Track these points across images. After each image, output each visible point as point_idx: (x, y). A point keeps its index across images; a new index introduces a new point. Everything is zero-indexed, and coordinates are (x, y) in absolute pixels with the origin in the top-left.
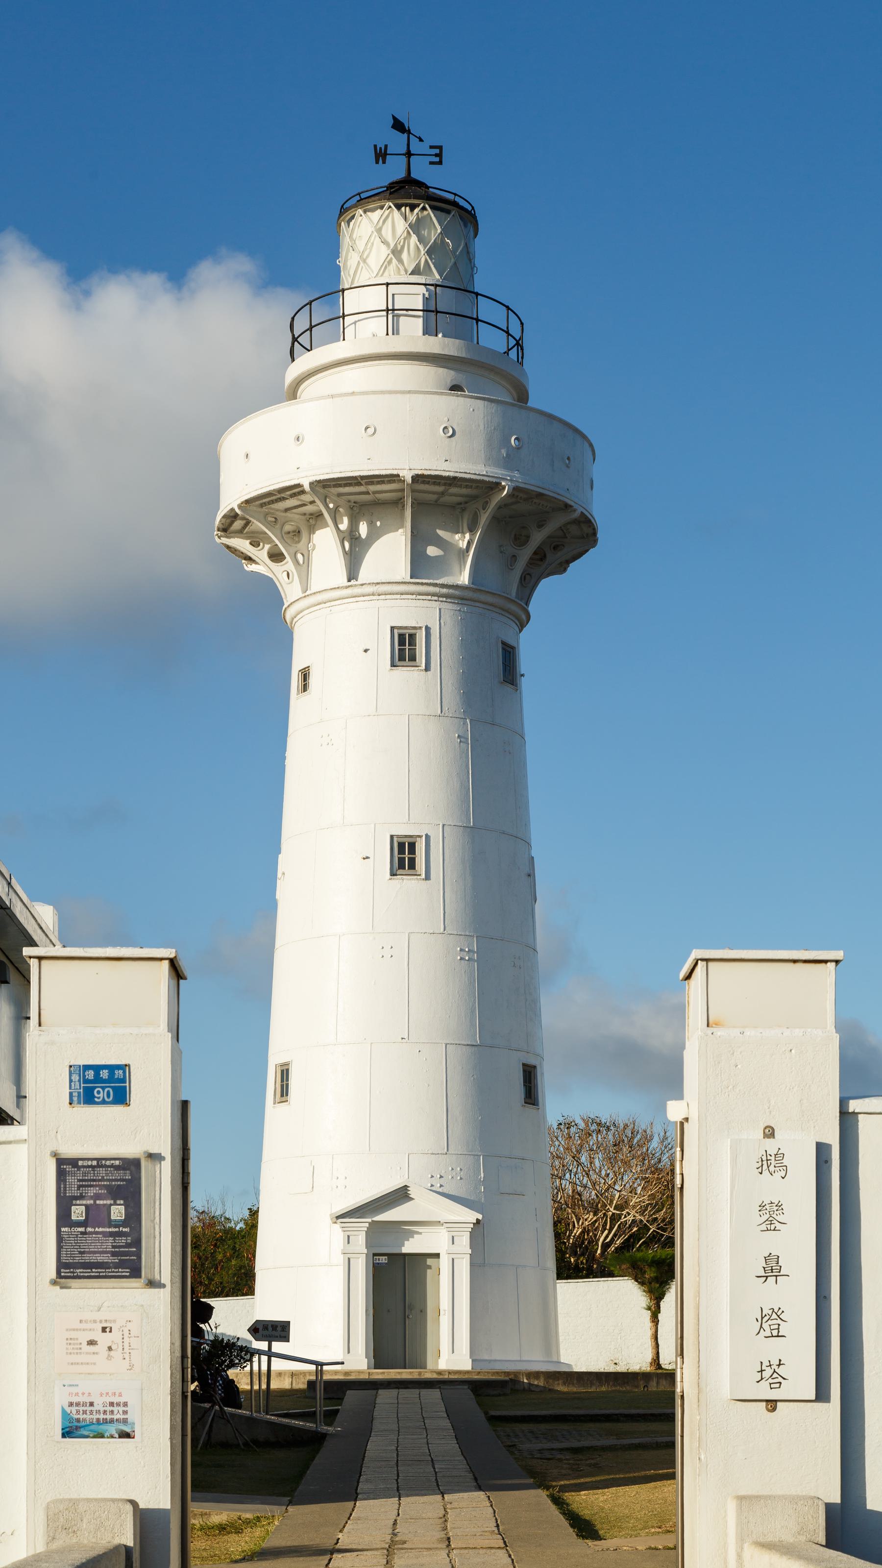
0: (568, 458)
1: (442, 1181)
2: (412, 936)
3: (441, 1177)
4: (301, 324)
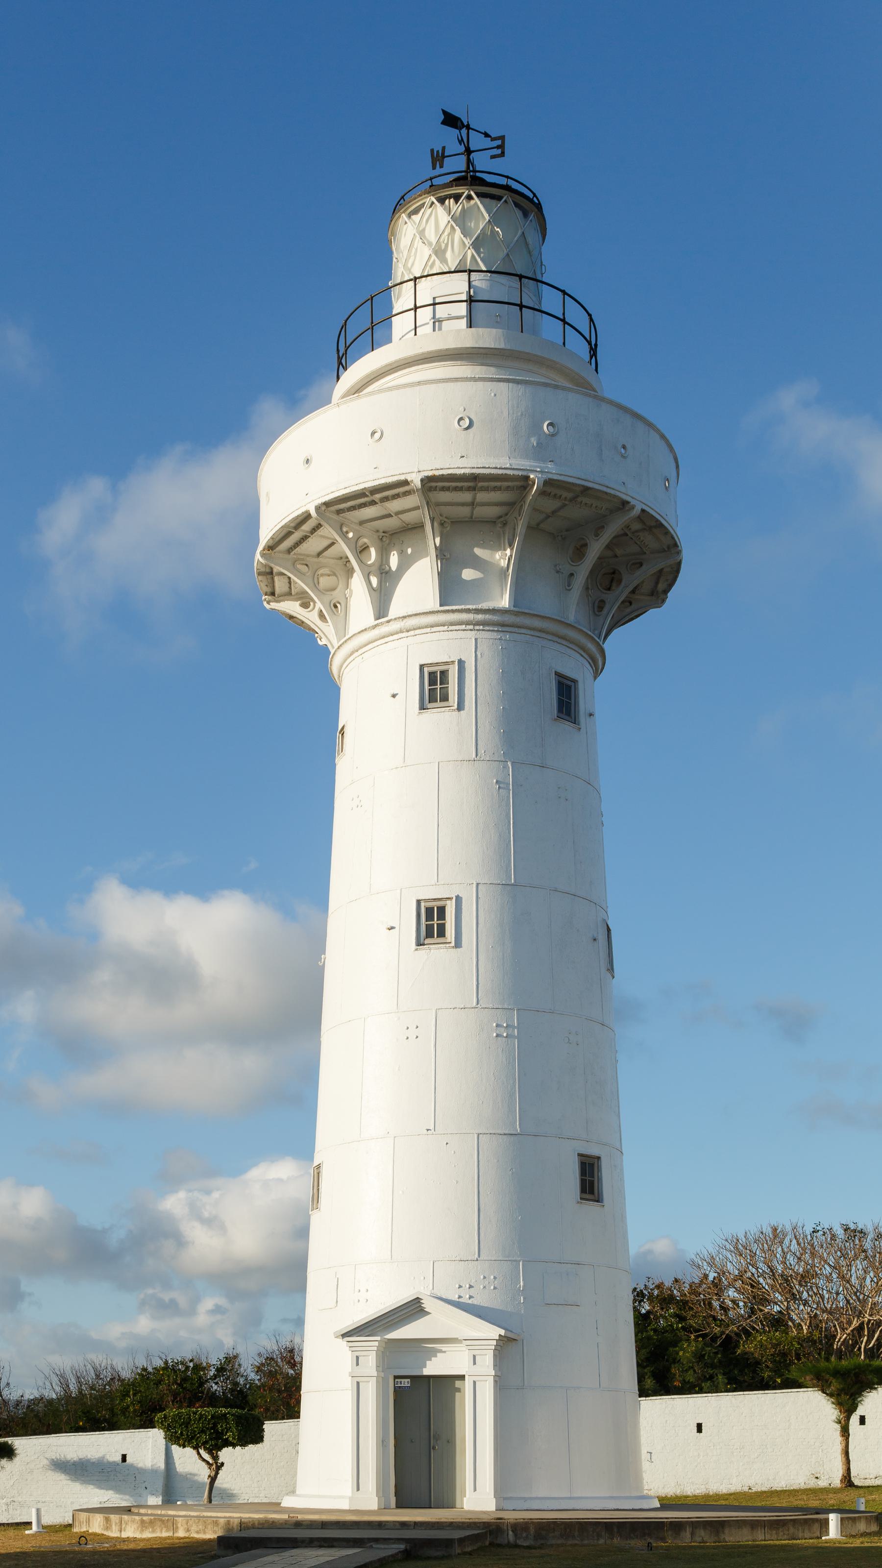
0: (624, 447)
1: (472, 1292)
2: (439, 1012)
3: (471, 1287)
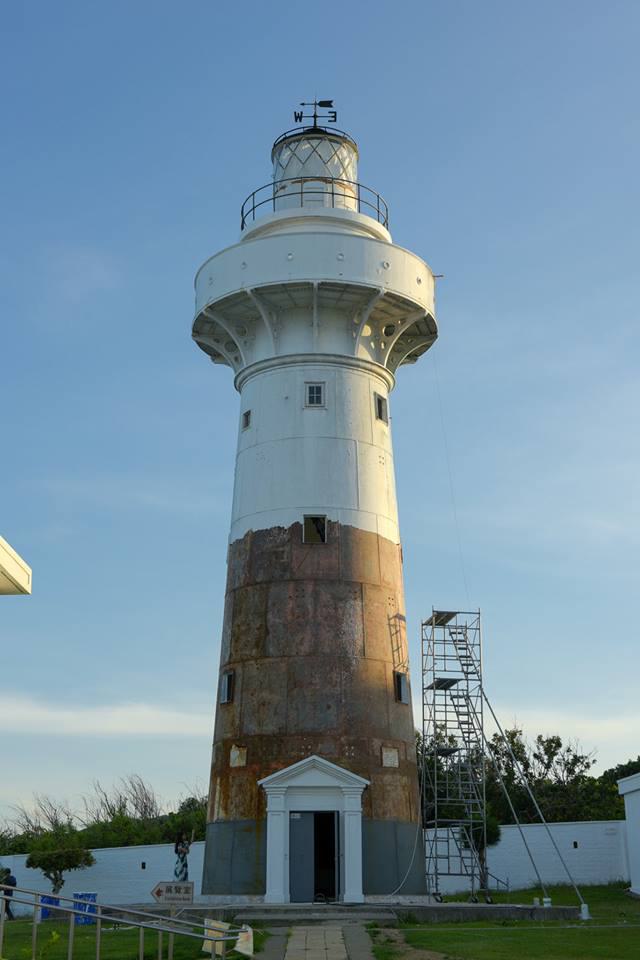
4: (249, 206)
